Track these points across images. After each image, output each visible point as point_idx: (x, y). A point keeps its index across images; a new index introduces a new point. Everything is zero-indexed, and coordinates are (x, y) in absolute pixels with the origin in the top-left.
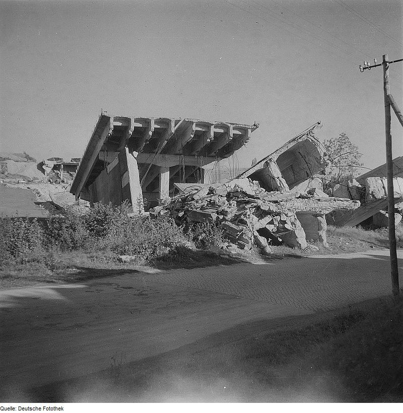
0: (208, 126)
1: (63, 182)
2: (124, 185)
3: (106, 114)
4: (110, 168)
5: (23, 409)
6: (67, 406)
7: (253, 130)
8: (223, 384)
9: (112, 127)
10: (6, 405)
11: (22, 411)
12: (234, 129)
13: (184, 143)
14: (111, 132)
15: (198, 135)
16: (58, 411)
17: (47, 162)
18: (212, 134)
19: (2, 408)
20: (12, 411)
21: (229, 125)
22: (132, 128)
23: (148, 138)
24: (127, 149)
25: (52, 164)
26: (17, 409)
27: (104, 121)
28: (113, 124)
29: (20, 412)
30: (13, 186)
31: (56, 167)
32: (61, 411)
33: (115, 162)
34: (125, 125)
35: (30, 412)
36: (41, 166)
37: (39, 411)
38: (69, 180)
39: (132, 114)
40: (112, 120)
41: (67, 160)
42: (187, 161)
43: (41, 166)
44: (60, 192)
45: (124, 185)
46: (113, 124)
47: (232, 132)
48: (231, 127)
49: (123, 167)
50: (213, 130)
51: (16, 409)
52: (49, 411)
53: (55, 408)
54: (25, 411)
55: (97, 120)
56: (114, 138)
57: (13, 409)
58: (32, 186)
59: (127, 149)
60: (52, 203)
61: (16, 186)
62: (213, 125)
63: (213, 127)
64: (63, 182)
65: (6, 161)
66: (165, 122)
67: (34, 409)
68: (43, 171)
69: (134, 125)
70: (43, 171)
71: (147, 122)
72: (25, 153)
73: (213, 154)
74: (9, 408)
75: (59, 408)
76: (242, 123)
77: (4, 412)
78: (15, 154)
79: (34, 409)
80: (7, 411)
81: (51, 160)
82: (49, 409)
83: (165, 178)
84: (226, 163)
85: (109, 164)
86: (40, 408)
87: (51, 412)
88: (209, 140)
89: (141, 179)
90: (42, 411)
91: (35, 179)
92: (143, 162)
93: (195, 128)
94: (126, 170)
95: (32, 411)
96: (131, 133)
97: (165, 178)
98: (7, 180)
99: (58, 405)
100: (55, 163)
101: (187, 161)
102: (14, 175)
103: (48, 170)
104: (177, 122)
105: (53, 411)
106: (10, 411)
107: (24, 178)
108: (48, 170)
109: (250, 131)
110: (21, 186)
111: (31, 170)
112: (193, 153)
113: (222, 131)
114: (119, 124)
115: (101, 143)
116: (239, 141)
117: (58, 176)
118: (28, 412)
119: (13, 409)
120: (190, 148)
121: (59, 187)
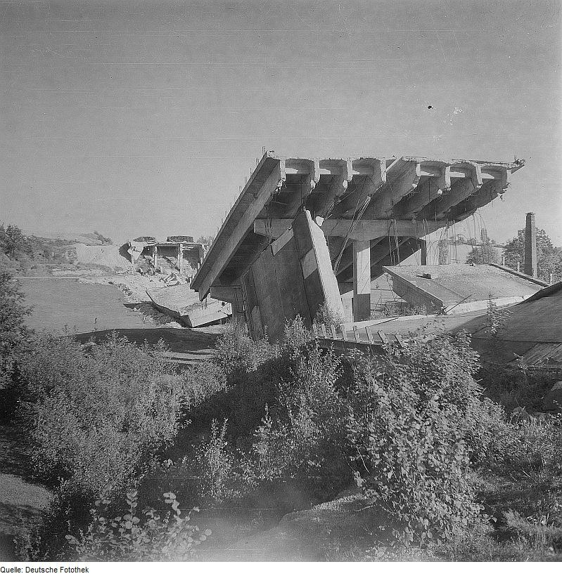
0: (439, 168)
1: (159, 271)
2: (308, 272)
3: (272, 155)
4: (277, 246)
5: (32, 570)
6: (96, 567)
7: (514, 170)
8: (281, 534)
9: (283, 176)
10: (9, 565)
11: (30, 574)
12: (483, 170)
13: (397, 199)
14: (280, 185)
15: (425, 183)
16: (81, 574)
17: (133, 244)
18: (448, 181)
19: (3, 570)
20: (17, 574)
21: (475, 165)
22: (317, 177)
23: (340, 193)
24: (308, 213)
25: (140, 247)
26: (24, 570)
27: (268, 167)
28: (285, 171)
29: (27, 574)
30: (88, 281)
31: (147, 251)
32: (85, 574)
33: (289, 235)
34: (438, 175)
35: (42, 574)
36: (125, 250)
37: (54, 574)
38: (188, 270)
39: (316, 154)
40: (282, 165)
41: (162, 240)
42: (399, 229)
43: (125, 250)
44: (175, 289)
45: (308, 272)
46: (285, 171)
47: (482, 176)
48: (479, 168)
49: (302, 244)
50: (449, 175)
51: (22, 570)
52: (68, 574)
53: (77, 569)
54: (35, 574)
55: (250, 168)
56: (287, 195)
57: (18, 570)
58: (117, 280)
59: (308, 213)
60: (153, 305)
61: (93, 281)
62: (448, 165)
63: (448, 169)
64: (159, 271)
65: (74, 246)
66: (368, 165)
67: (48, 570)
68: (129, 257)
69: (319, 172)
70: (129, 257)
71: (307, 165)
72: (96, 233)
73: (441, 215)
74: (12, 569)
75: (83, 569)
76: (495, 159)
77: (6, 574)
78: (85, 235)
79: (48, 570)
80: (10, 574)
81: (139, 240)
82: (68, 570)
83: (363, 259)
84: (466, 228)
85: (273, 240)
86: (56, 569)
87: (71, 574)
88: (440, 192)
89: (333, 262)
90: (58, 573)
91: (118, 269)
92: (335, 234)
93: (420, 172)
94: (309, 246)
95: (45, 574)
96: (313, 184)
97: (363, 259)
98: (78, 273)
99: (81, 565)
100: (146, 244)
101: (399, 229)
102: (88, 264)
103: (136, 255)
104: (389, 163)
105: (74, 574)
106: (14, 574)
107: (103, 268)
108: (136, 255)
109: (508, 172)
110: (100, 281)
111: (112, 257)
112: (408, 216)
113: (462, 175)
114: (294, 171)
115: (258, 206)
116: (491, 190)
117: (150, 264)
118: (39, 574)
119: (18, 570)
120: (403, 208)
121: (155, 279)
